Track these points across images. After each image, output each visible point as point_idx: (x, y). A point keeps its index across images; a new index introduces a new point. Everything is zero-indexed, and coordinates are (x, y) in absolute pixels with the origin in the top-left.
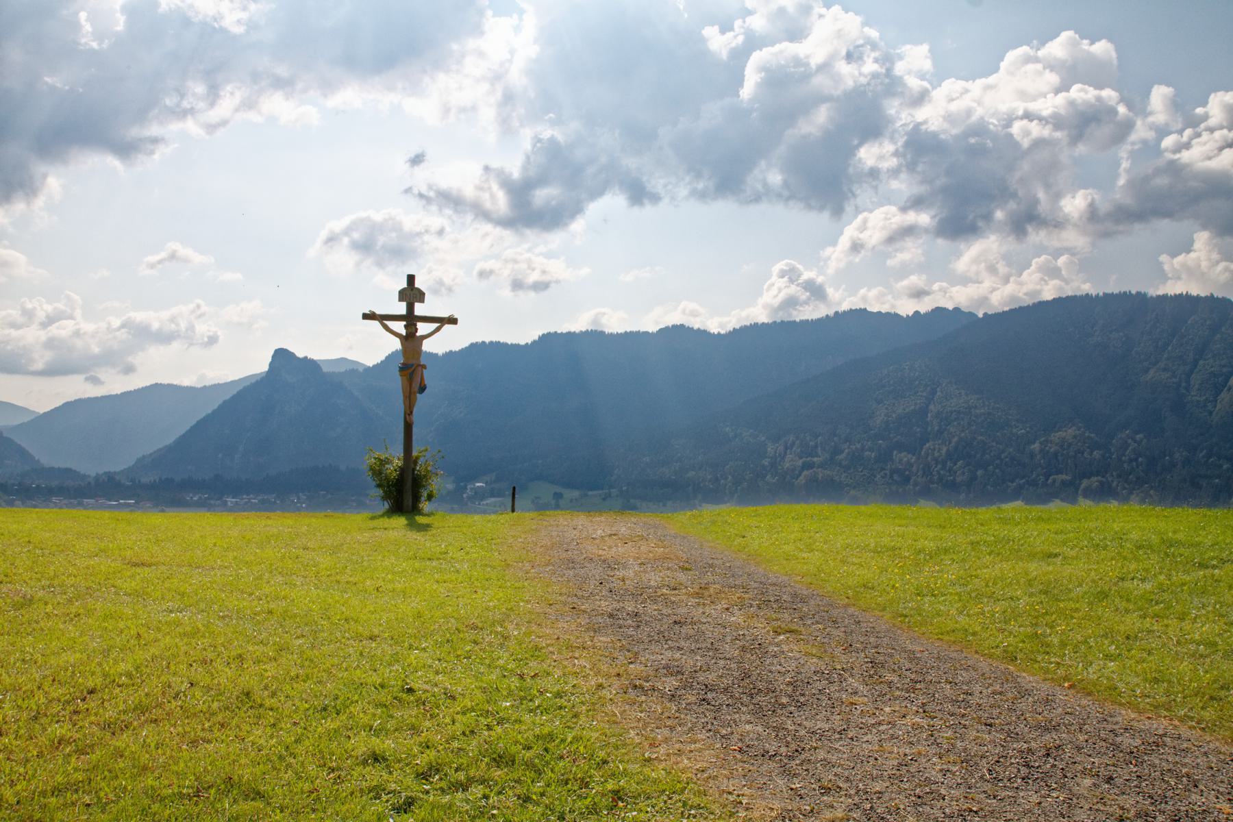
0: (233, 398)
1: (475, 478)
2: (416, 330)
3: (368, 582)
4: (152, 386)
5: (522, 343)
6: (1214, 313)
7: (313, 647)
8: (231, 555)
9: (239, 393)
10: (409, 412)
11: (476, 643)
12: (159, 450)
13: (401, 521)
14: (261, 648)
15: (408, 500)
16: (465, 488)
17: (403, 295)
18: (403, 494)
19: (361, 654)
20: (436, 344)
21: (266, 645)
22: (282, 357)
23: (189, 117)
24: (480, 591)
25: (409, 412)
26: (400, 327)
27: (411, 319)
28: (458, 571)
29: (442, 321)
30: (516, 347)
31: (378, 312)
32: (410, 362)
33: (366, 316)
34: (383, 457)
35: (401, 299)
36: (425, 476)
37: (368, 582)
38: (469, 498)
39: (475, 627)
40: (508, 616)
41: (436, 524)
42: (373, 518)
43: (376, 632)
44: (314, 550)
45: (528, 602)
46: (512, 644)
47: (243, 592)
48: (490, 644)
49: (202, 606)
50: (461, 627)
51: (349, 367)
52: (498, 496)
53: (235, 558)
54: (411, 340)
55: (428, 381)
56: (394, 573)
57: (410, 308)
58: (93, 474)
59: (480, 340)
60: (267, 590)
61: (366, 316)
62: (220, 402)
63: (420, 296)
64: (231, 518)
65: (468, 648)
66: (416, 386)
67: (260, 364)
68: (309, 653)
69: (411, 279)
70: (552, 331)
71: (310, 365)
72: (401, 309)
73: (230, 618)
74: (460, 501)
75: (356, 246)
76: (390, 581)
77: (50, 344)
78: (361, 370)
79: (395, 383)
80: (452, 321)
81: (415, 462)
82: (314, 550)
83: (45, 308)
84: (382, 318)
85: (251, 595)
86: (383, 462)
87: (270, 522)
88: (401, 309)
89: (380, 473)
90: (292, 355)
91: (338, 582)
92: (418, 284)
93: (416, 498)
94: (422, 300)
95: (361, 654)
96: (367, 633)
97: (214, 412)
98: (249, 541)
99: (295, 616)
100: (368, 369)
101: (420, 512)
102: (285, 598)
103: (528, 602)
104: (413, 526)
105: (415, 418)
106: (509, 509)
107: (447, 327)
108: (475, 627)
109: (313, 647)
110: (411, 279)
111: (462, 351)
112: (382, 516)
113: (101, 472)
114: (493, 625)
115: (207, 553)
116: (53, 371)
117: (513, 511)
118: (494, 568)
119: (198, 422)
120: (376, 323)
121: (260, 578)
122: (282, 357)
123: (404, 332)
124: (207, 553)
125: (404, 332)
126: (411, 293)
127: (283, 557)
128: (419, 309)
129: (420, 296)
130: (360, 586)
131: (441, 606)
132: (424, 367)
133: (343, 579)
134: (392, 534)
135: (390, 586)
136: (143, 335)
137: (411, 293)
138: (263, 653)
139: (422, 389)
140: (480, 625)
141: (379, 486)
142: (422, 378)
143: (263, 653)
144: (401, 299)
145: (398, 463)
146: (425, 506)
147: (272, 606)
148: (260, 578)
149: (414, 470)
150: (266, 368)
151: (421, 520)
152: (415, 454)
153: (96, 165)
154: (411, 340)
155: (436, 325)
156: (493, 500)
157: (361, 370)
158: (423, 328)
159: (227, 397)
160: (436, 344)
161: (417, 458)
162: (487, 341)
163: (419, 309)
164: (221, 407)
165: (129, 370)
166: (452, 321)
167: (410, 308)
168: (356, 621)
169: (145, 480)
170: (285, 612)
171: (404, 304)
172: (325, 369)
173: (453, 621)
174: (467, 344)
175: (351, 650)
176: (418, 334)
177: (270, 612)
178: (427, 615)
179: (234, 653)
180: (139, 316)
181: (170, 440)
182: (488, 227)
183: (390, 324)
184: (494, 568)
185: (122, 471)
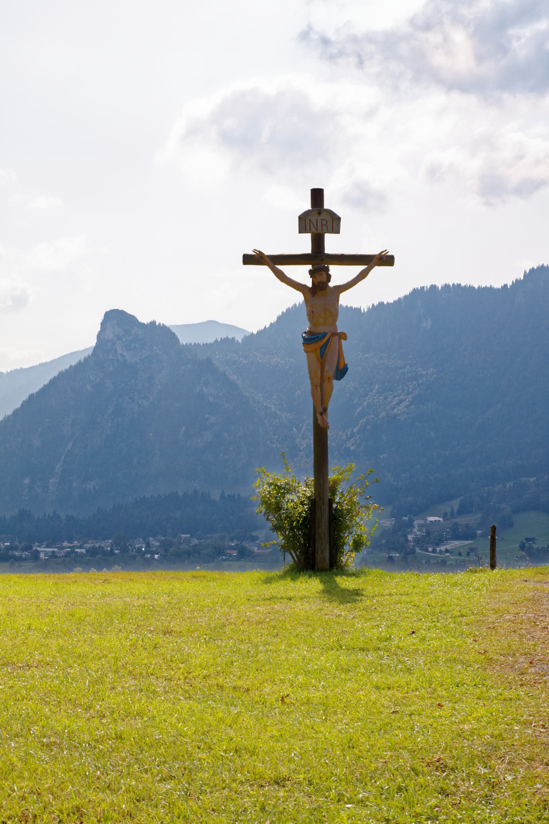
0: (45, 390)
1: (422, 510)
2: (329, 277)
3: (267, 688)
5: (498, 285)
7: (188, 795)
8: (54, 643)
9: (53, 381)
10: (321, 410)
11: (443, 792)
13: (312, 585)
14: (109, 797)
15: (323, 554)
16: (410, 525)
17: (305, 223)
18: (315, 543)
19: (263, 809)
20: (364, 295)
21: (115, 792)
22: (117, 322)
23: (337, 542)
24: (448, 705)
25: (321, 410)
26: (302, 274)
27: (318, 260)
28: (409, 671)
29: (369, 261)
30: (489, 291)
31: (268, 251)
32: (321, 329)
33: (248, 260)
34: (282, 482)
35: (302, 230)
36: (349, 511)
37: (267, 688)
38: (417, 541)
39: (442, 767)
40: (496, 748)
41: (369, 590)
42: (268, 581)
43: (284, 771)
44: (180, 634)
45: (527, 724)
46: (505, 798)
47: (75, 706)
48: (468, 796)
49: (16, 727)
50: (420, 766)
51: (220, 336)
52: (466, 537)
53: (61, 649)
54: (320, 293)
55: (349, 358)
56: (307, 673)
57: (318, 242)
59: (427, 284)
60: (113, 700)
61: (248, 260)
63: (333, 223)
64: (50, 583)
65: (434, 802)
66: (330, 370)
67: (82, 336)
68: (182, 806)
69: (317, 195)
71: (160, 333)
72: (303, 244)
73: (60, 746)
74: (402, 552)
75: (228, 140)
76: (302, 686)
78: (239, 339)
79: (300, 359)
80: (386, 260)
81: (333, 491)
82: (180, 634)
84: (275, 262)
85: (88, 708)
86: (283, 490)
87: (109, 589)
88: (303, 244)
89: (278, 508)
90: (132, 319)
91: (221, 687)
92: (330, 203)
93: (336, 547)
94: (336, 230)
95: (263, 809)
96: (269, 774)
97: (16, 413)
98: (81, 621)
99: (157, 744)
101: (342, 570)
102: (140, 714)
103: (527, 724)
104: (333, 593)
105: (332, 418)
106: (487, 560)
107: (377, 270)
108: (442, 767)
109: (188, 795)
110: (317, 195)
111: (399, 302)
112: (282, 577)
114: (471, 763)
115: (18, 641)
117: (493, 566)
118: (467, 664)
120: (264, 270)
121: (100, 681)
122: (117, 322)
123: (308, 282)
124: (18, 641)
125: (308, 282)
126: (319, 219)
127: (134, 646)
128: (333, 244)
129: (333, 223)
130: (255, 695)
131: (385, 729)
132: (343, 336)
133: (228, 682)
134: (301, 608)
135: (303, 695)
137: (319, 219)
138: (112, 804)
139: (341, 372)
140: (450, 763)
141: (278, 528)
142: (340, 355)
143: (112, 804)
144: (302, 230)
145: (305, 490)
146: (349, 558)
147: (121, 727)
148: (100, 681)
149: (331, 501)
150: (92, 342)
151: (345, 583)
152: (332, 476)
154: (320, 293)
155: (358, 269)
156: (457, 543)
157: (239, 339)
158: (339, 274)
159: (35, 389)
160: (364, 295)
161: (336, 483)
162: (440, 285)
163: (333, 244)
164: (25, 404)
166: (386, 260)
167: (318, 242)
168: (253, 753)
170: (143, 737)
171: (307, 237)
172: (183, 340)
173: (405, 753)
174: (407, 292)
175: (247, 802)
176: (331, 284)
177: (119, 737)
178: (364, 743)
179: (67, 805)
182: (437, 98)
183: (287, 269)
184: (467, 664)
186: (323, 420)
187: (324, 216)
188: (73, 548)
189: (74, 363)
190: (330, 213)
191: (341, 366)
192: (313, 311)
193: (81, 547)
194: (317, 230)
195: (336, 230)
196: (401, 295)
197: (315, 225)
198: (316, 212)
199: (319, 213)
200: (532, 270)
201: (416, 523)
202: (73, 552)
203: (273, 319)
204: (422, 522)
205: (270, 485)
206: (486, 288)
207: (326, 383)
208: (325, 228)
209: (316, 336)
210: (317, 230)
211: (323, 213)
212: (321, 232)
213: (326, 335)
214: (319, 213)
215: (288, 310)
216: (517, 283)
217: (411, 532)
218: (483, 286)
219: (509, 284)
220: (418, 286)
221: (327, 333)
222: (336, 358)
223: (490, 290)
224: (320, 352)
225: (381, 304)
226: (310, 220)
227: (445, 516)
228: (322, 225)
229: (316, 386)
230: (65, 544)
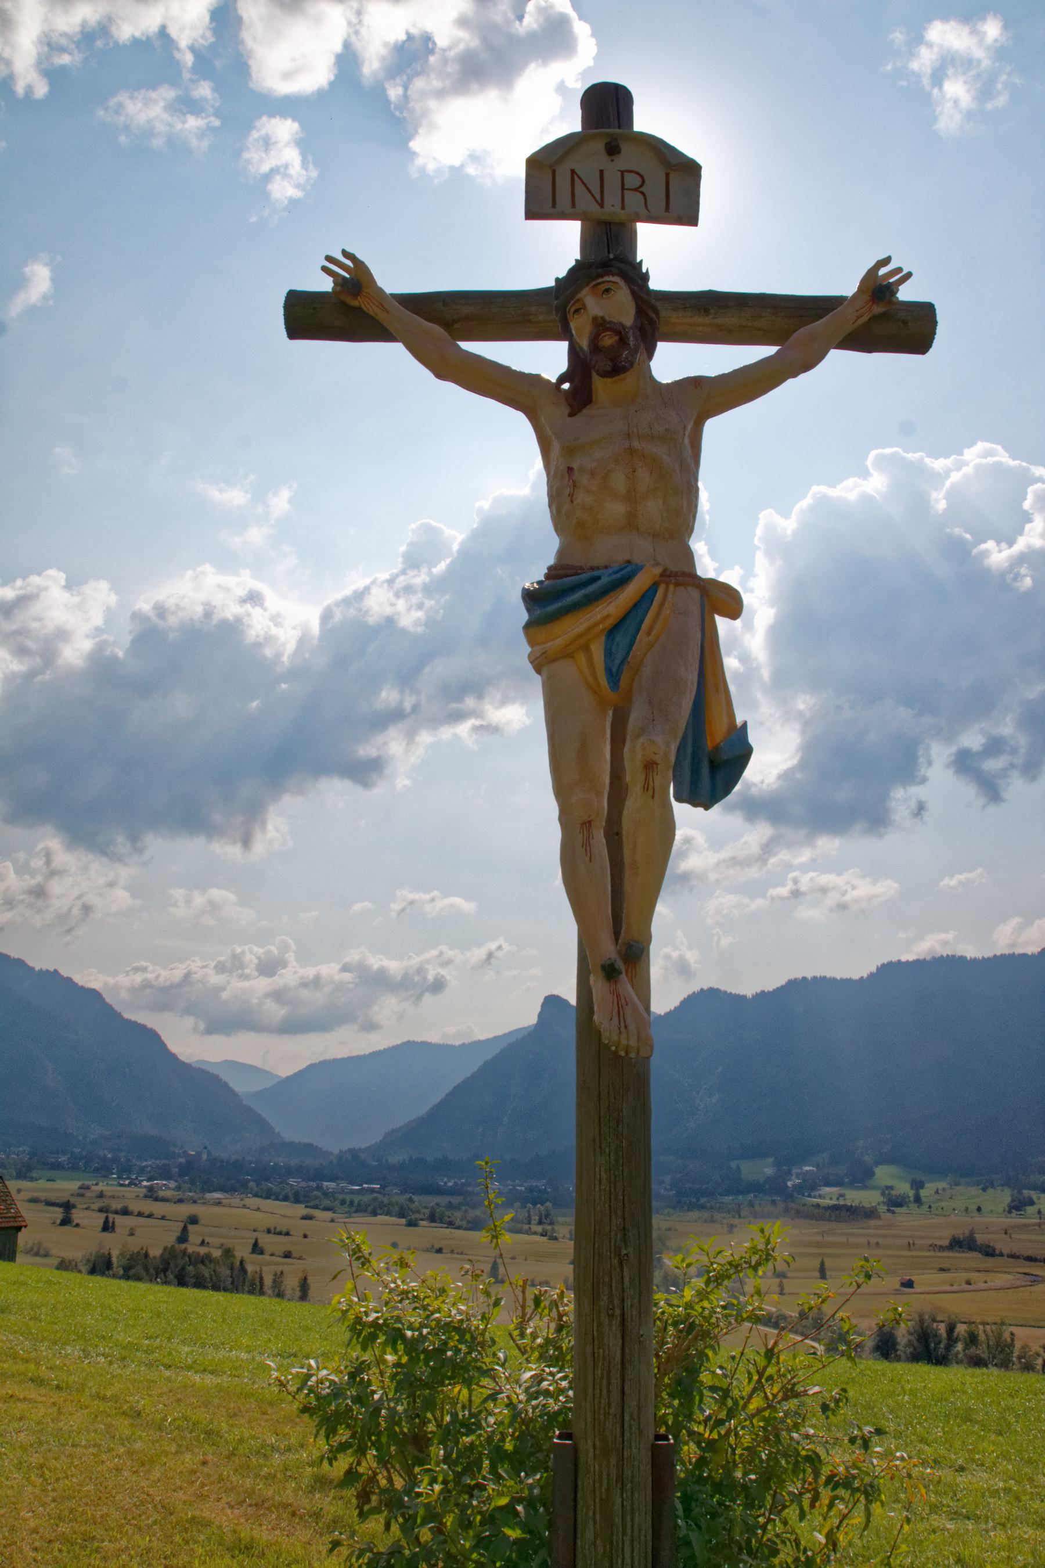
4: (404, 1044)
6: (935, 1002)
12: (410, 1122)
22: (56, 971)
27: (608, 315)
32: (607, 551)
57: (610, 255)
58: (336, 1151)
59: (799, 976)
62: (480, 1063)
63: (673, 186)
70: (894, 959)
77: (278, 996)
83: (252, 954)
94: (686, 213)
100: (537, 1025)
113: (345, 1148)
116: (293, 1027)
119: (455, 1088)
122: (56, 971)
128: (667, 257)
129: (673, 186)
136: (378, 982)
153: (336, 793)
159: (489, 1057)
161: (696, 1333)
162: (809, 976)
165: (371, 1026)
169: (393, 1160)
180: (375, 962)
181: (422, 1111)
185: (369, 1148)
186: (620, 1007)
187: (629, 157)
188: (515, 1186)
189: (519, 1037)
190: (658, 149)
191: (717, 733)
192: (570, 469)
193: (521, 1186)
194: (601, 205)
195: (686, 213)
196: (779, 985)
197: (599, 199)
198: (600, 146)
199: (612, 150)
200: (883, 965)
201: (795, 1171)
202: (515, 1189)
203: (677, 1003)
204: (799, 1171)
205: (364, 1333)
206: (847, 980)
207: (633, 803)
208: (633, 200)
209: (584, 576)
210: (601, 205)
211: (626, 148)
212: (622, 215)
213: (624, 581)
214: (612, 150)
215: (689, 996)
216: (871, 976)
217: (790, 1180)
218: (844, 977)
219: (865, 976)
220: (792, 977)
221: (639, 568)
222: (693, 678)
223: (849, 981)
224: (608, 654)
225: (763, 992)
226: (573, 172)
227: (818, 1166)
228: (623, 188)
229: (588, 824)
230: (509, 1182)
